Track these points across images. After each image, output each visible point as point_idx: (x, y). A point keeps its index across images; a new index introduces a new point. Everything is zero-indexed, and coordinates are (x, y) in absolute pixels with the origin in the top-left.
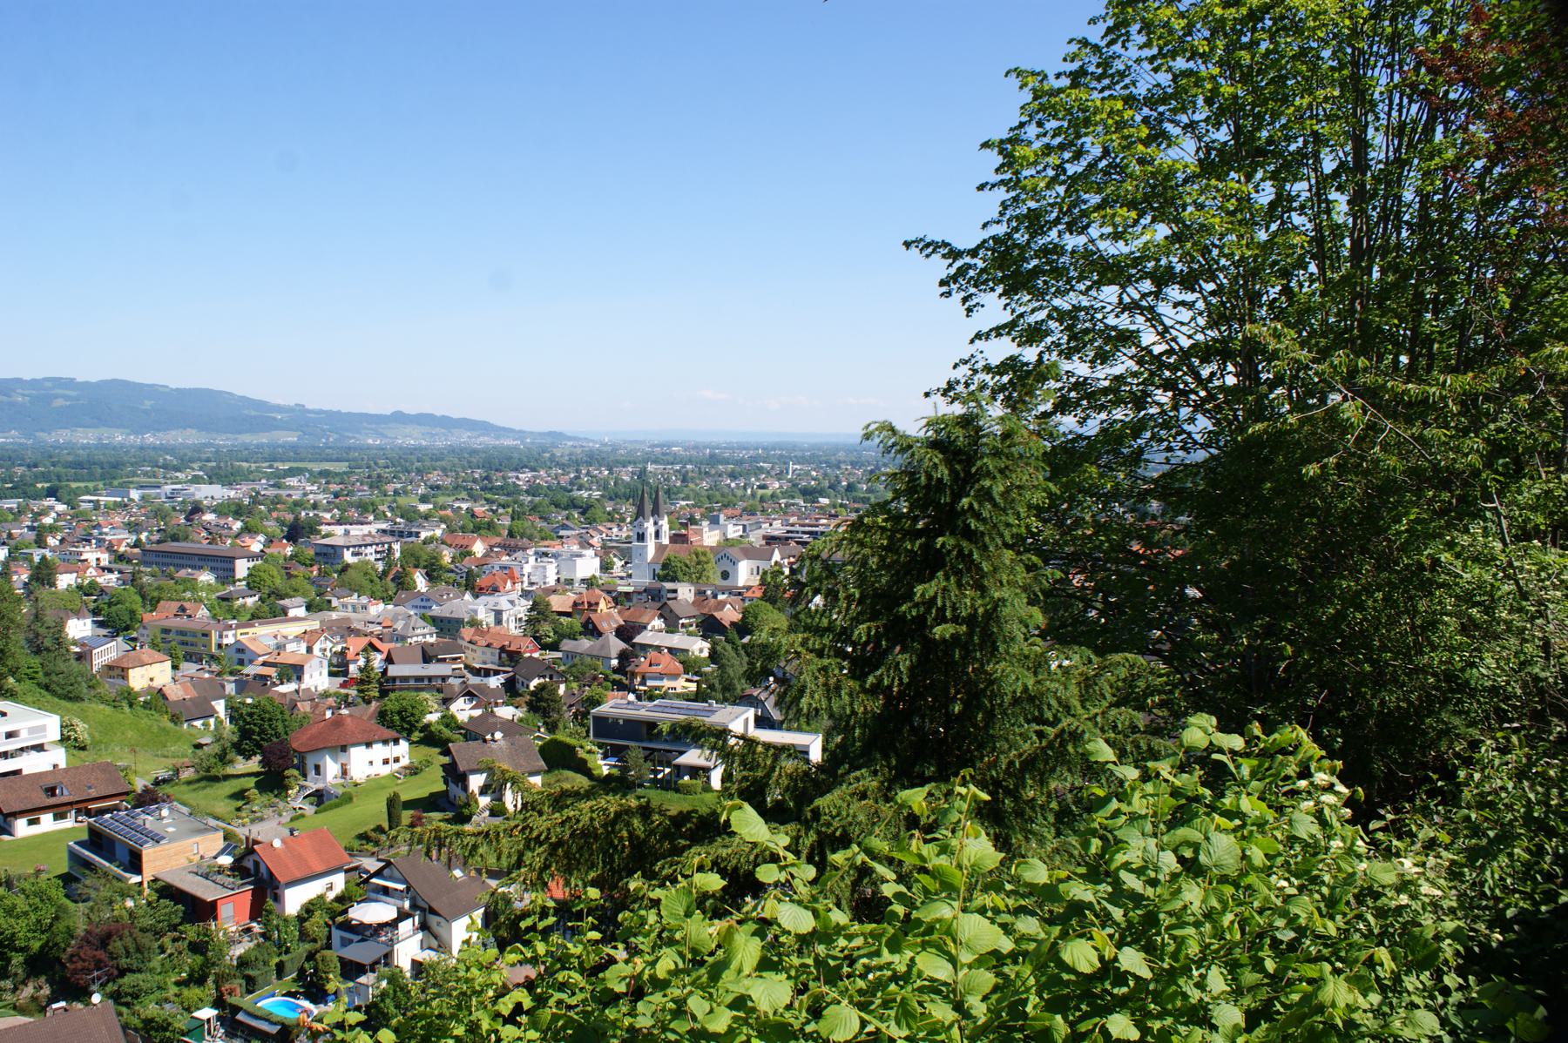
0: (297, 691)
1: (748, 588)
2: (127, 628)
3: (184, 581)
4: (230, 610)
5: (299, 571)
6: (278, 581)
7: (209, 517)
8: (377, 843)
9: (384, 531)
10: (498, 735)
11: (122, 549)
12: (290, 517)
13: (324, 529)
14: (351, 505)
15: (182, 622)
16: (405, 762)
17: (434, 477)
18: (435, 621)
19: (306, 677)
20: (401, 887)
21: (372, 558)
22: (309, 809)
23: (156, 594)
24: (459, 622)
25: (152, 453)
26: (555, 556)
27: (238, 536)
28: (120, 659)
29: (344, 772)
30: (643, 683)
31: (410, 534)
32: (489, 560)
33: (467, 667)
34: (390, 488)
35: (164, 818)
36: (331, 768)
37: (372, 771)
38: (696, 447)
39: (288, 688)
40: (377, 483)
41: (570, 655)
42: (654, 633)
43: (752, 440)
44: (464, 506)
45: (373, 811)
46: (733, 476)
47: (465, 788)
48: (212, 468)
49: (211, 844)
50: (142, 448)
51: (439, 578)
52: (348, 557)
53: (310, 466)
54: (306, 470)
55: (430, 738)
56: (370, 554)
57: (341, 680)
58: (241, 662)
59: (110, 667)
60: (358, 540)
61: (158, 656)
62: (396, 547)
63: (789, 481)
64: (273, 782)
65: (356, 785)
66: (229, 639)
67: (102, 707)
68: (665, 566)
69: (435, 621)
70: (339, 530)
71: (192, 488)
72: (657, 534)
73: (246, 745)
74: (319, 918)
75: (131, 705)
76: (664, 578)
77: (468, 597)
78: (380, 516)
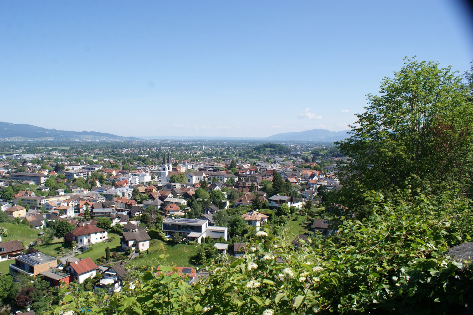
0: (66, 218)
1: (196, 184)
2: (9, 199)
3: (25, 184)
4: (41, 193)
5: (61, 181)
6: (55, 184)
7: (29, 164)
8: (103, 262)
9: (84, 168)
10: (136, 230)
11: (4, 174)
12: (55, 164)
13: (66, 168)
14: (73, 160)
15: (26, 197)
16: (106, 238)
17: (97, 151)
18: (104, 195)
19: (68, 213)
20: (115, 274)
21: (82, 176)
22: (80, 253)
23: (18, 188)
24: (112, 196)
25: (8, 144)
26: (138, 175)
27: (40, 170)
28: (10, 209)
29: (89, 241)
30: (169, 213)
31: (92, 169)
32: (118, 177)
33: (116, 209)
34: (84, 154)
35: (39, 256)
36: (85, 240)
37: (97, 241)
38: (174, 141)
39: (64, 216)
40: (79, 153)
41: (146, 205)
42: (170, 198)
43: (191, 139)
44: (107, 160)
45: (101, 252)
46: (186, 150)
47: (128, 245)
48: (28, 149)
49: (54, 264)
50: (5, 142)
51: (103, 182)
52: (75, 176)
53: (58, 148)
54: (57, 149)
55: (113, 231)
56: (82, 175)
57: (78, 213)
58: (48, 209)
59: (7, 211)
60: (76, 170)
61: (22, 207)
62: (90, 173)
63: (203, 151)
64: (68, 244)
65: (93, 245)
66: (43, 202)
67: (10, 224)
68: (171, 178)
69: (104, 195)
70: (70, 168)
71: (23, 155)
72: (168, 169)
73: (59, 234)
74: (89, 285)
75: (18, 223)
76: (171, 182)
77: (113, 188)
78: (82, 164)
